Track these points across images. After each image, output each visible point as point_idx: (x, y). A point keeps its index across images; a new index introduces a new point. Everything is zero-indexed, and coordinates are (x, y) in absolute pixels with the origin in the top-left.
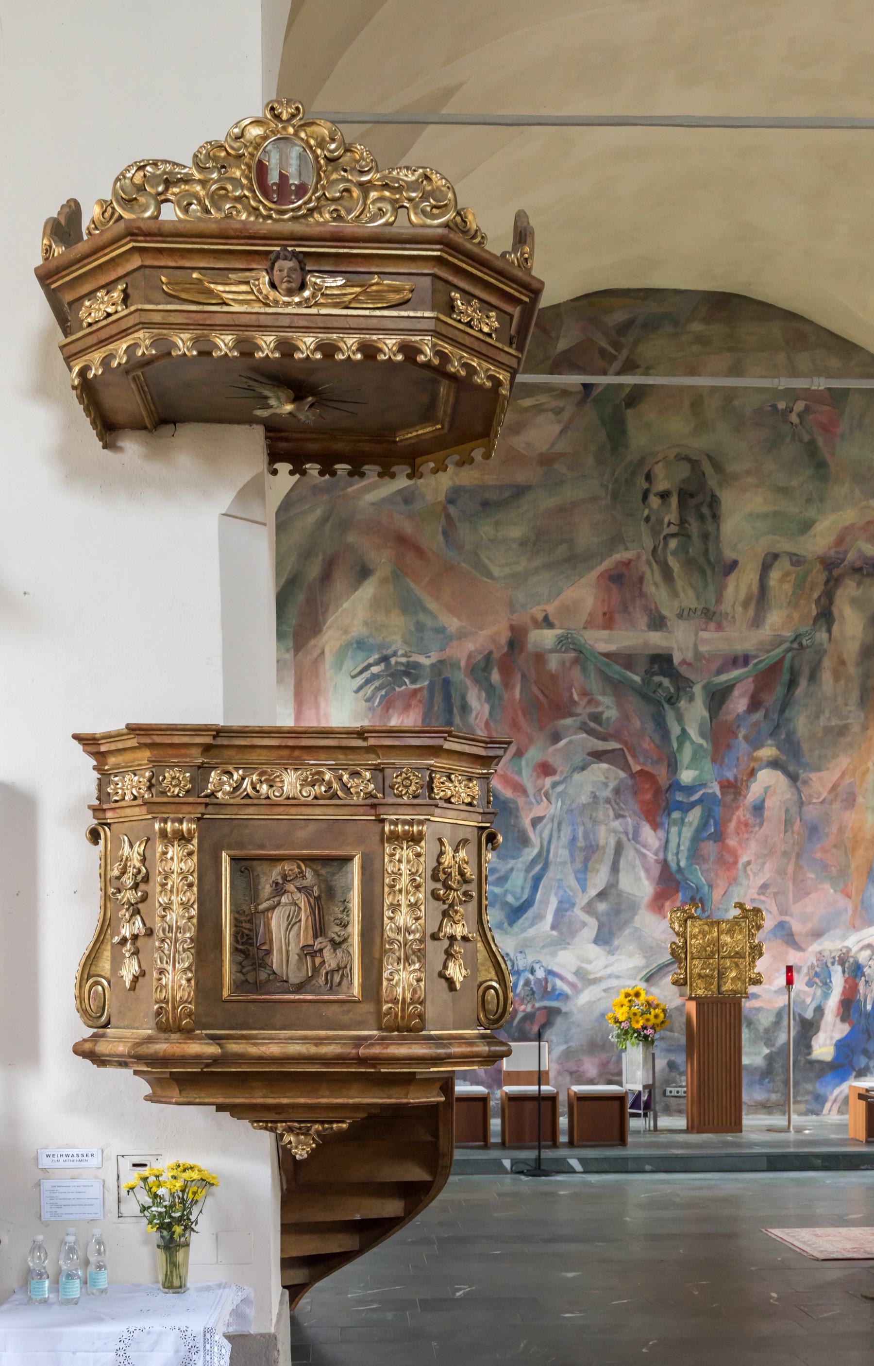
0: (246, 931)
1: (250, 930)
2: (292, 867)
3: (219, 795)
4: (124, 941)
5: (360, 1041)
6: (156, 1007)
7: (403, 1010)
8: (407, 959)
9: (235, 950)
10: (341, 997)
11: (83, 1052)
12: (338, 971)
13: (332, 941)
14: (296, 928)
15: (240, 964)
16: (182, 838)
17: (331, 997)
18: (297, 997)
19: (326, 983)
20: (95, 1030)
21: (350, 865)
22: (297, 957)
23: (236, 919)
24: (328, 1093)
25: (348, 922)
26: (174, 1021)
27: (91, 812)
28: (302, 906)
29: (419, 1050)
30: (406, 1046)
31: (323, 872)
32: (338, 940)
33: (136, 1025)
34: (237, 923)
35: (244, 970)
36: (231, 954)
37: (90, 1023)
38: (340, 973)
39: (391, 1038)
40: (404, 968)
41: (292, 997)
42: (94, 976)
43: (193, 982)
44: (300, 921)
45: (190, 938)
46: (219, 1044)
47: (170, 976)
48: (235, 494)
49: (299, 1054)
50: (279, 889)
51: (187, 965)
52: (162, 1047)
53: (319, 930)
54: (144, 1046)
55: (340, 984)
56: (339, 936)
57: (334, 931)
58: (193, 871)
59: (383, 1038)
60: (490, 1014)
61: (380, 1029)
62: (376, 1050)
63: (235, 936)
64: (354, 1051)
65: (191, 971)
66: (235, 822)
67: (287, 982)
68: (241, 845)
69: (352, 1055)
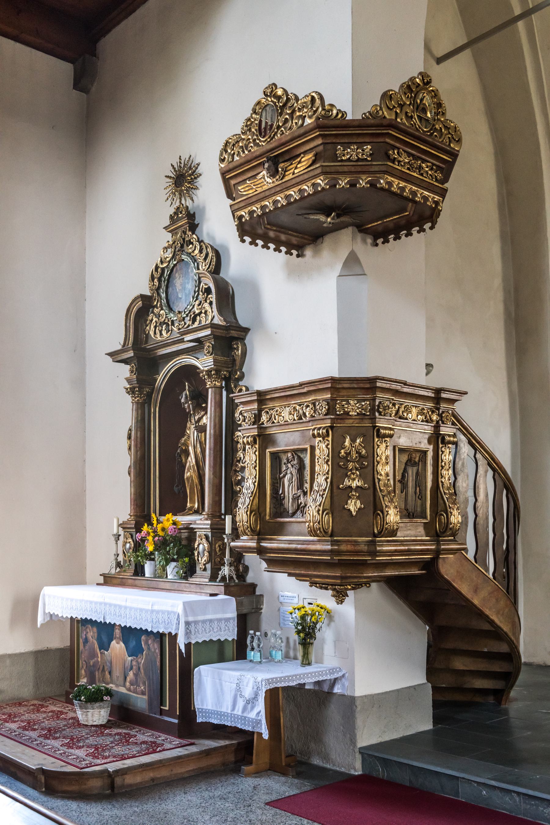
15: (274, 504)
48: (342, 265)
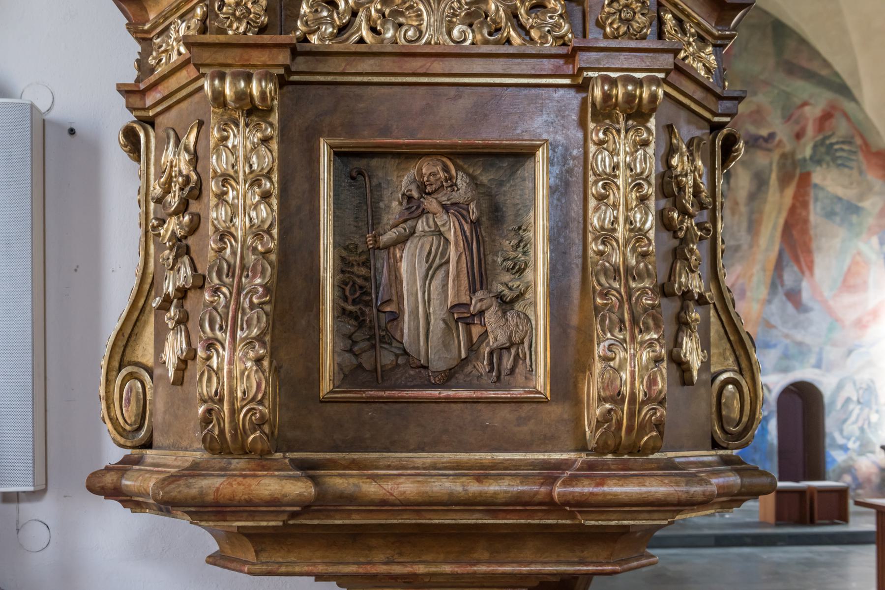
0: (359, 281)
1: (367, 279)
2: (434, 170)
3: (314, 39)
4: (167, 302)
5: (551, 472)
6: (201, 410)
7: (631, 415)
8: (634, 321)
9: (341, 313)
10: (517, 393)
11: (103, 488)
12: (508, 349)
13: (500, 297)
14: (441, 274)
16: (253, 111)
17: (501, 394)
18: (445, 393)
19: (491, 371)
20: (128, 452)
21: (529, 164)
22: (442, 325)
23: (343, 259)
24: (486, 555)
25: (526, 264)
26: (235, 436)
27: (122, 100)
28: (452, 238)
29: (657, 488)
30: (635, 480)
31: (484, 179)
32: (509, 295)
33: (184, 444)
34: (343, 266)
35: (356, 349)
36: (334, 318)
37: (122, 441)
38: (513, 351)
39: (604, 466)
40: (633, 337)
41: (435, 393)
42: (131, 363)
43: (266, 363)
44: (448, 262)
45: (265, 286)
46: (312, 478)
47: (226, 354)
49: (451, 494)
50: (414, 209)
51: (255, 332)
52: (211, 485)
53: (479, 278)
54: (181, 482)
55: (512, 371)
56: (510, 289)
57: (503, 282)
58: (271, 171)
59: (591, 466)
60: (729, 424)
61: (582, 448)
62: (584, 489)
63: (341, 286)
64: (543, 489)
65: (263, 344)
66: (342, 89)
67: (426, 368)
68: (350, 129)
69: (539, 498)
